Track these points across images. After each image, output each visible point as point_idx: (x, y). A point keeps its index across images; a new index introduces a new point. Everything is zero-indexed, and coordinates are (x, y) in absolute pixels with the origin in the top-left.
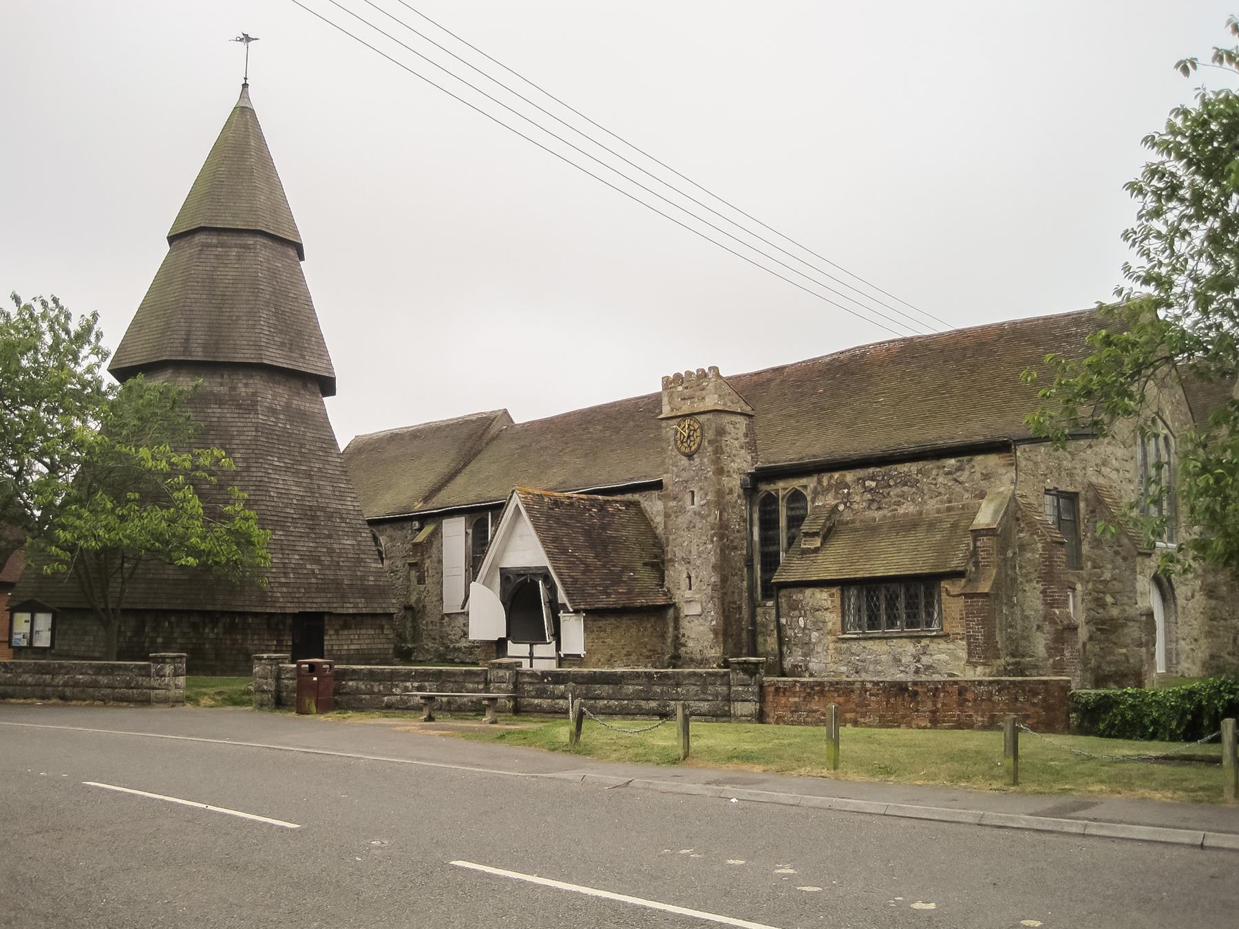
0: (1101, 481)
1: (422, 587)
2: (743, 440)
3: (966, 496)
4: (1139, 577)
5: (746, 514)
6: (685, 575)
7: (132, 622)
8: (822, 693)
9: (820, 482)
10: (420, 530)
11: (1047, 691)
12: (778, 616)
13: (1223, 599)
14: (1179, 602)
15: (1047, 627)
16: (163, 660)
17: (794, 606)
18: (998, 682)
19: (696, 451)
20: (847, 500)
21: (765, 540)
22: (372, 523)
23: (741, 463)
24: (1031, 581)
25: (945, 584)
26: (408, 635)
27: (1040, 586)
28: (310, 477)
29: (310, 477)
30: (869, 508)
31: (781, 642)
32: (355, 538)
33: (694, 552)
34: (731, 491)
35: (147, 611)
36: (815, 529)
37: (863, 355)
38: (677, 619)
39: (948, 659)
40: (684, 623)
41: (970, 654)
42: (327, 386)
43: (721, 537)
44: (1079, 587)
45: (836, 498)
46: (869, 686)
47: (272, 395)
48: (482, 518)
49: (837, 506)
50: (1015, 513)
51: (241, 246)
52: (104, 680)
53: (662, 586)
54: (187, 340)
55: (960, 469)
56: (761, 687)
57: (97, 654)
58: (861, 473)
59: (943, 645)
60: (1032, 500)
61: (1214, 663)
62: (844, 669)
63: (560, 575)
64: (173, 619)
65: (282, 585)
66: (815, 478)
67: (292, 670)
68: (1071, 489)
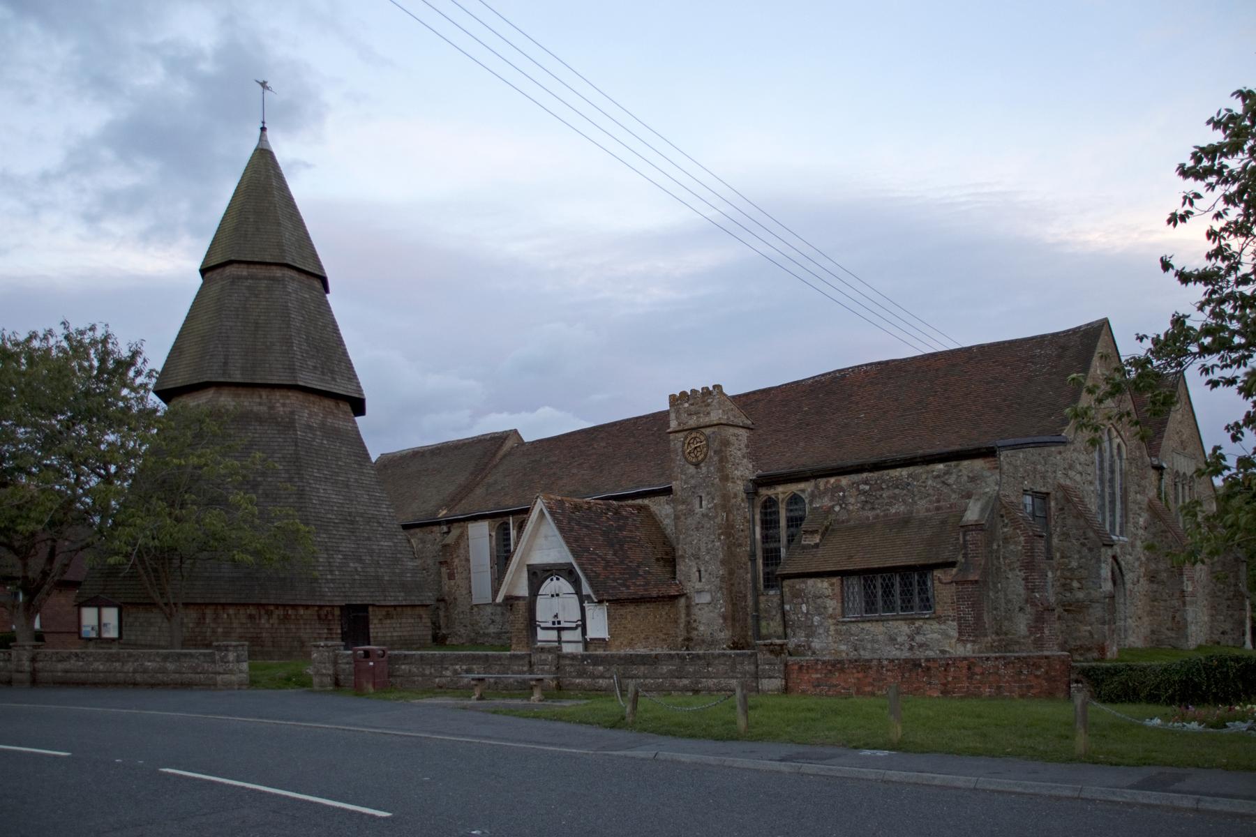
0: (1068, 482)
1: (452, 582)
2: (745, 450)
3: (954, 496)
4: (1103, 565)
5: (748, 516)
6: (695, 570)
7: (193, 614)
8: (842, 670)
9: (817, 487)
10: (448, 533)
11: (1049, 665)
12: (783, 603)
13: (1163, 583)
15: (1028, 608)
16: (226, 648)
17: (797, 594)
18: (1004, 658)
19: (703, 460)
21: (765, 538)
22: (406, 527)
23: (744, 471)
24: (1014, 569)
25: (937, 573)
26: (443, 625)
27: (1022, 574)
28: (347, 486)
29: (347, 486)
30: (863, 509)
33: (703, 549)
34: (736, 496)
35: (207, 605)
36: (814, 527)
37: (844, 377)
38: (688, 607)
39: (940, 637)
40: (695, 610)
41: (960, 633)
42: (358, 406)
43: (728, 535)
44: (1050, 574)
45: (832, 500)
46: (885, 663)
47: (310, 413)
49: (833, 507)
50: (999, 509)
51: (270, 279)
52: (170, 666)
53: (674, 578)
54: (226, 364)
55: (947, 473)
56: (786, 665)
57: (162, 643)
59: (936, 626)
60: (1013, 499)
61: (1155, 637)
62: (843, 647)
63: (584, 570)
64: (231, 611)
65: (327, 581)
67: (348, 656)
68: (1044, 490)
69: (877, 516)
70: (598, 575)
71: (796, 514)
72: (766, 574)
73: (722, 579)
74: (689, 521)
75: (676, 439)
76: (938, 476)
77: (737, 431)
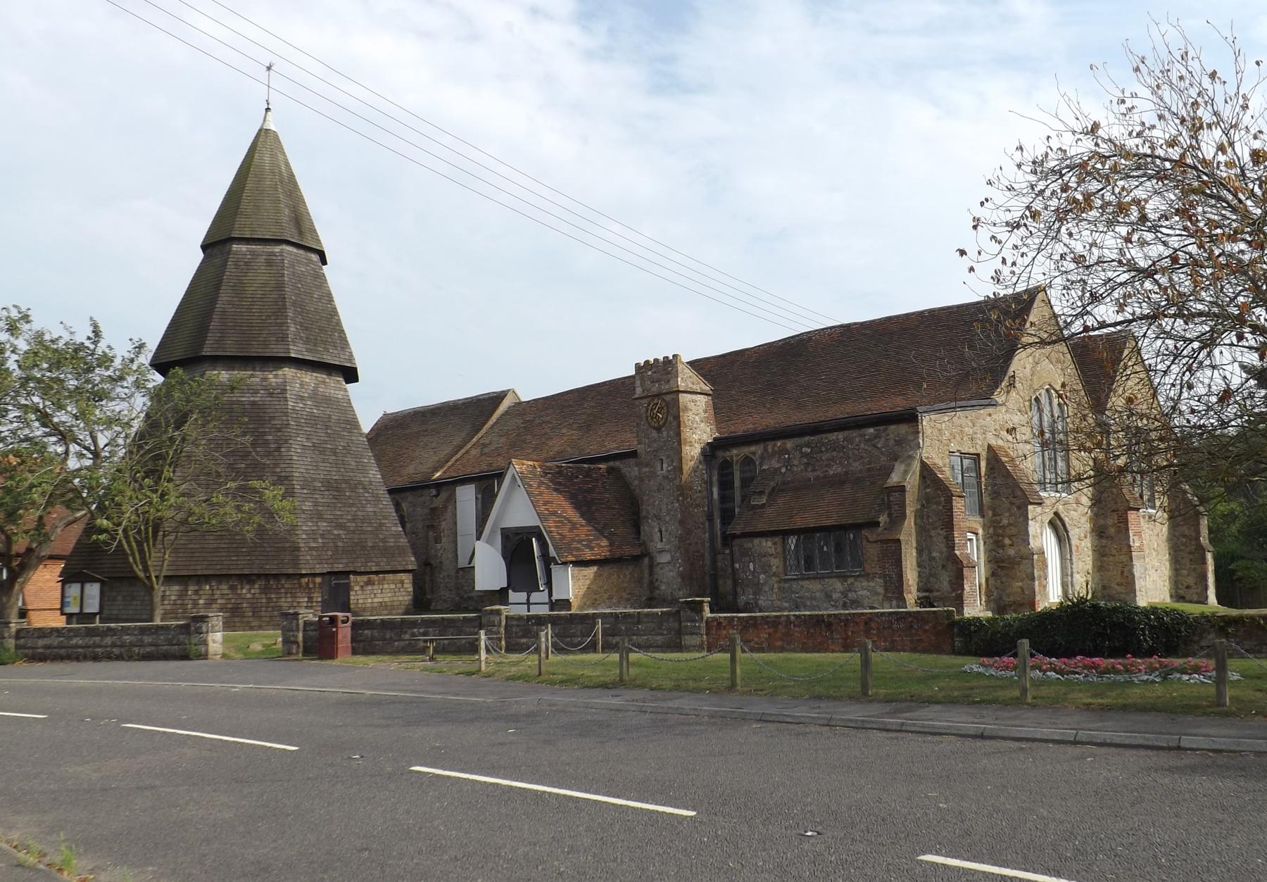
0: (1000, 443)
2: (703, 415)
9: (765, 450)
10: (436, 496)
12: (733, 562)
14: (1073, 542)
20: (787, 463)
21: (723, 498)
25: (865, 532)
28: (335, 454)
29: (335, 454)
31: (735, 583)
32: (375, 506)
38: (651, 566)
40: (657, 570)
41: (886, 590)
48: (488, 484)
49: (780, 468)
53: (638, 539)
55: (877, 436)
58: (798, 441)
59: (865, 584)
66: (762, 446)
69: (817, 478)
70: (563, 537)
71: (749, 475)
72: (723, 533)
73: (681, 538)
74: (652, 482)
75: (641, 404)
76: (869, 440)
77: (694, 397)
